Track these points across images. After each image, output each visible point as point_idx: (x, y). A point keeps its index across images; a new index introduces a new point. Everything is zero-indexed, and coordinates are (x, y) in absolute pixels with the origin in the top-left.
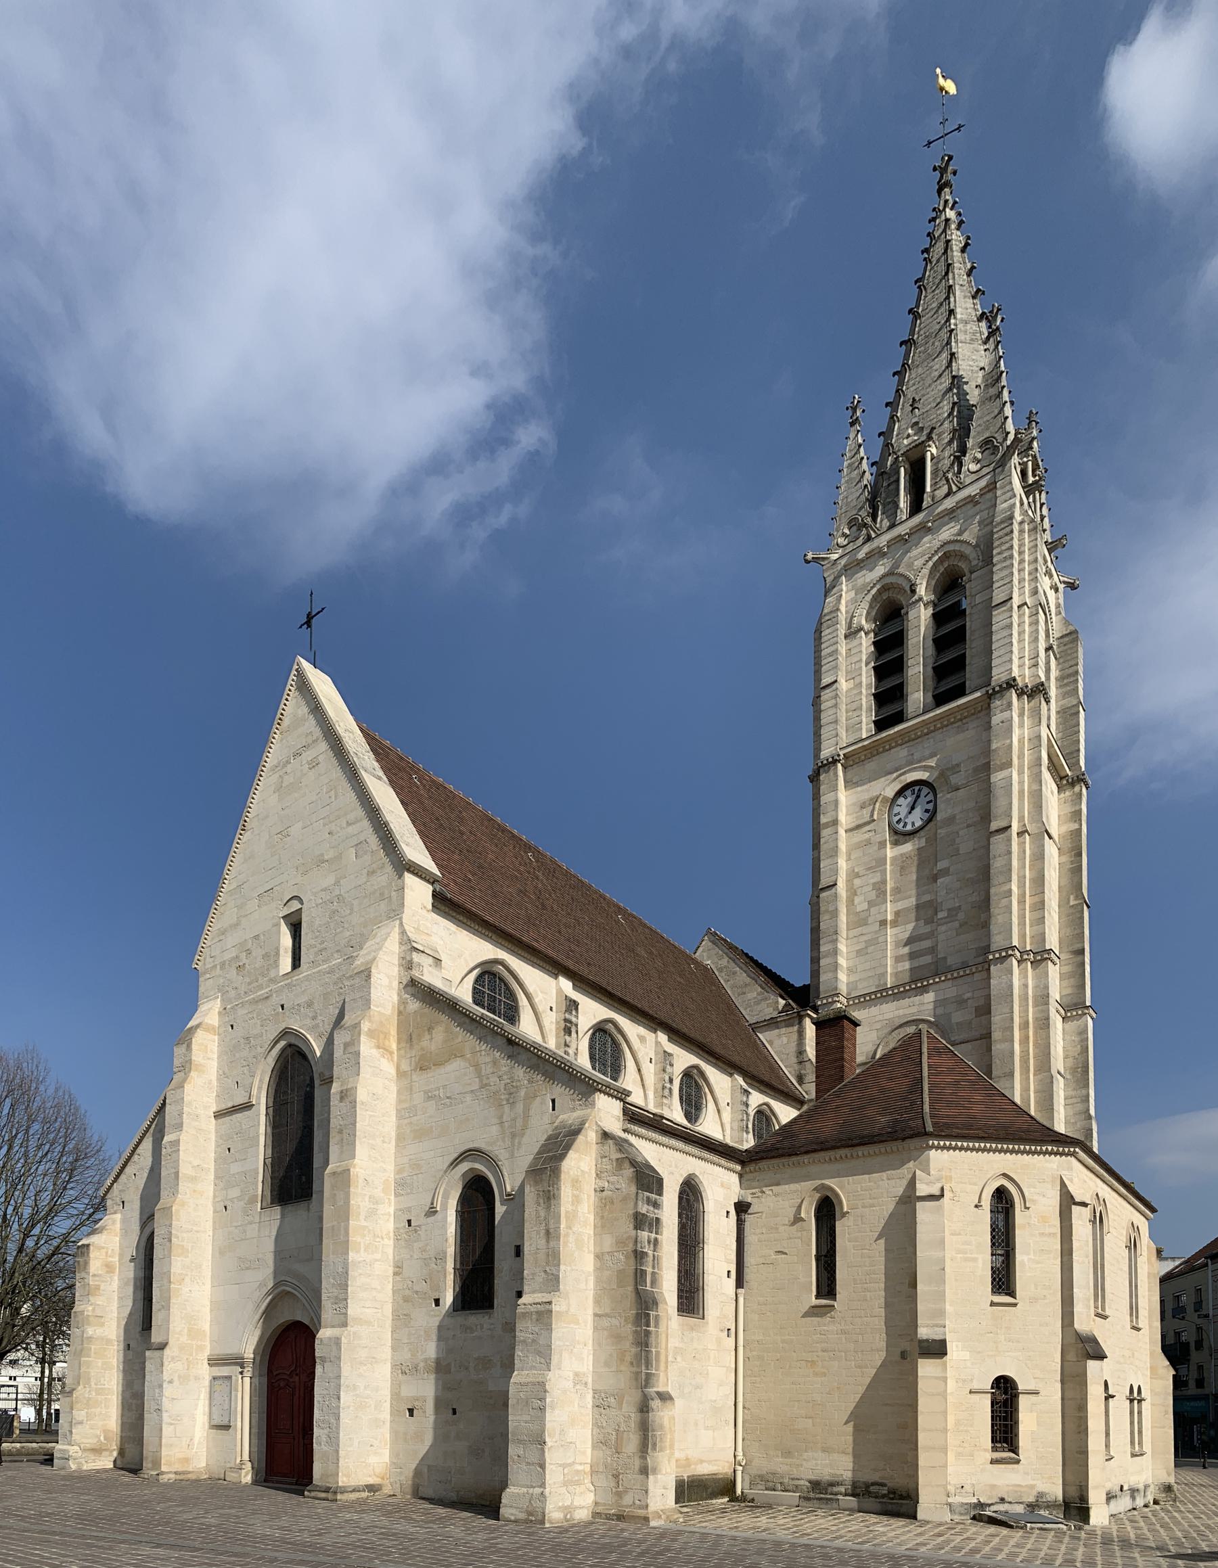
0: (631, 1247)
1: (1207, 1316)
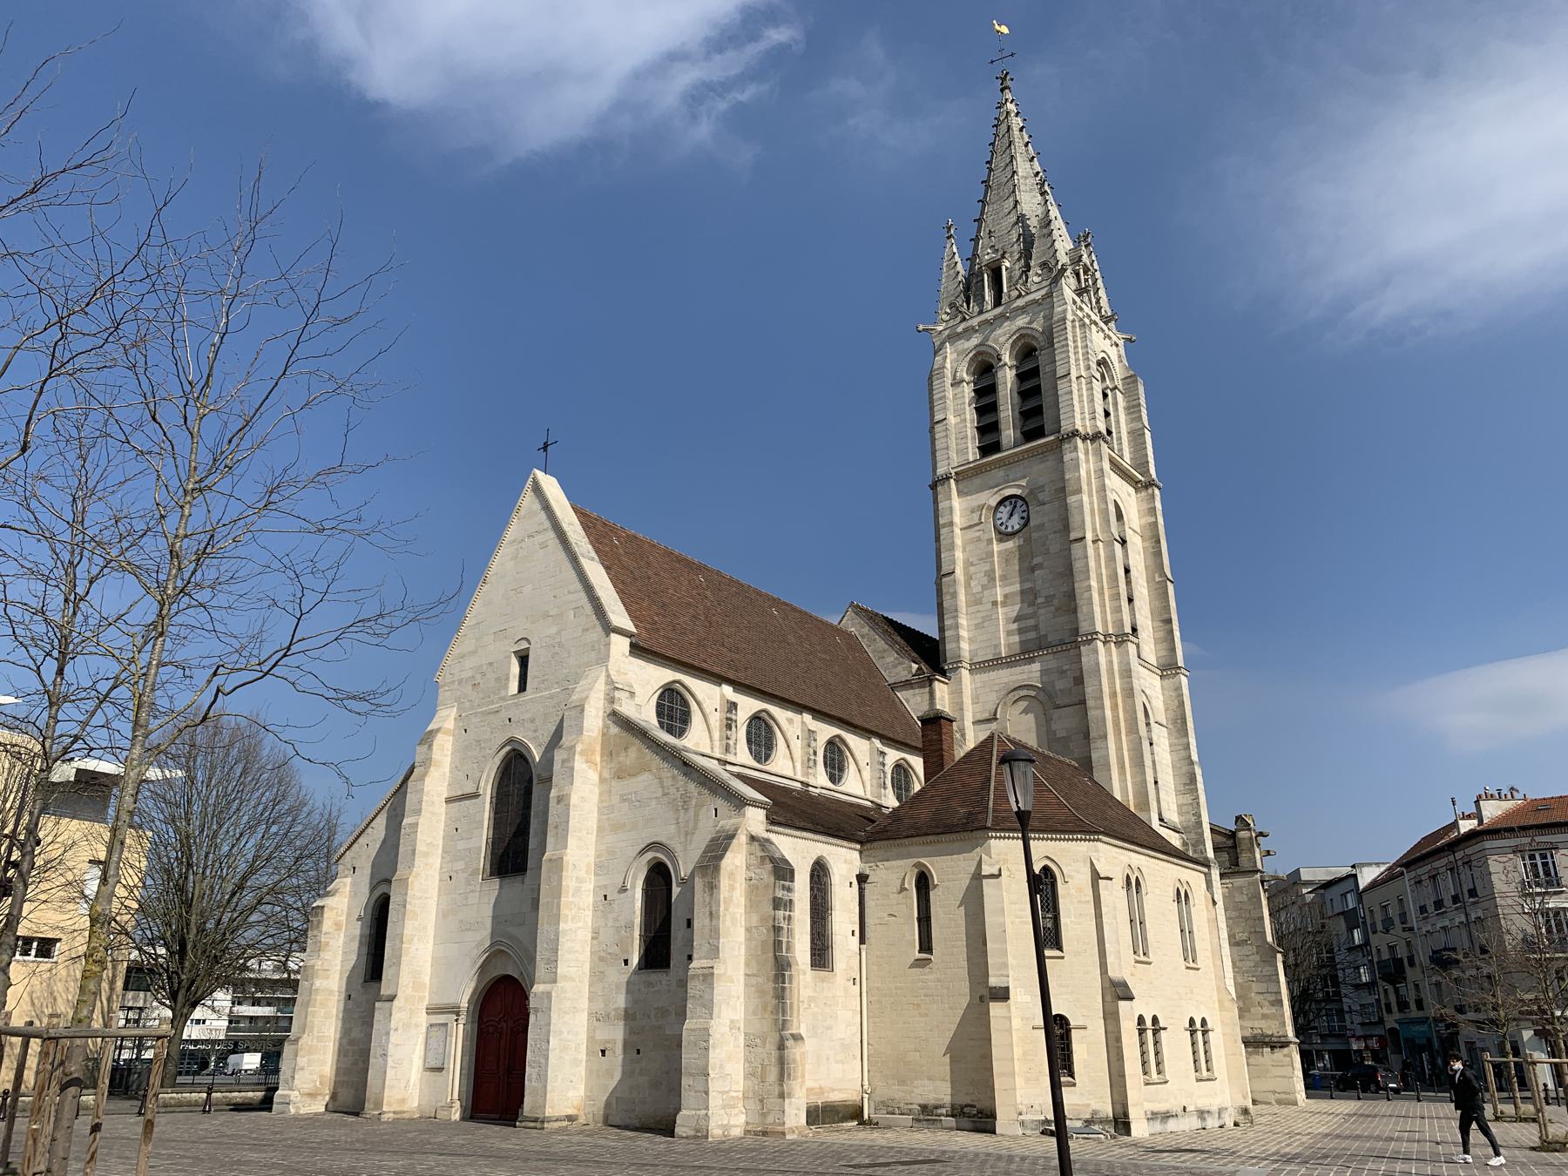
0: (771, 923)
1: (1411, 929)
